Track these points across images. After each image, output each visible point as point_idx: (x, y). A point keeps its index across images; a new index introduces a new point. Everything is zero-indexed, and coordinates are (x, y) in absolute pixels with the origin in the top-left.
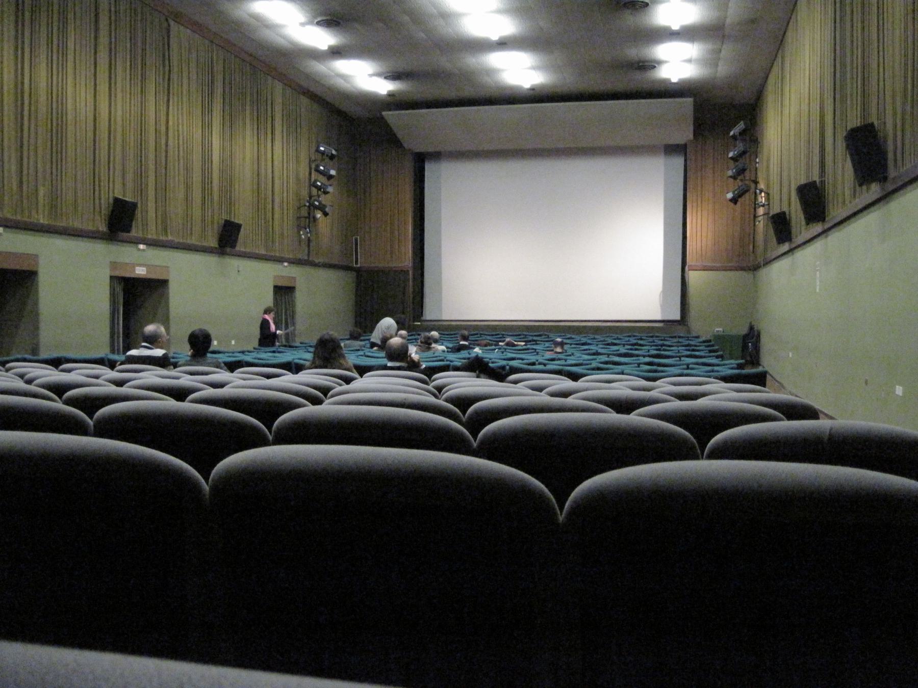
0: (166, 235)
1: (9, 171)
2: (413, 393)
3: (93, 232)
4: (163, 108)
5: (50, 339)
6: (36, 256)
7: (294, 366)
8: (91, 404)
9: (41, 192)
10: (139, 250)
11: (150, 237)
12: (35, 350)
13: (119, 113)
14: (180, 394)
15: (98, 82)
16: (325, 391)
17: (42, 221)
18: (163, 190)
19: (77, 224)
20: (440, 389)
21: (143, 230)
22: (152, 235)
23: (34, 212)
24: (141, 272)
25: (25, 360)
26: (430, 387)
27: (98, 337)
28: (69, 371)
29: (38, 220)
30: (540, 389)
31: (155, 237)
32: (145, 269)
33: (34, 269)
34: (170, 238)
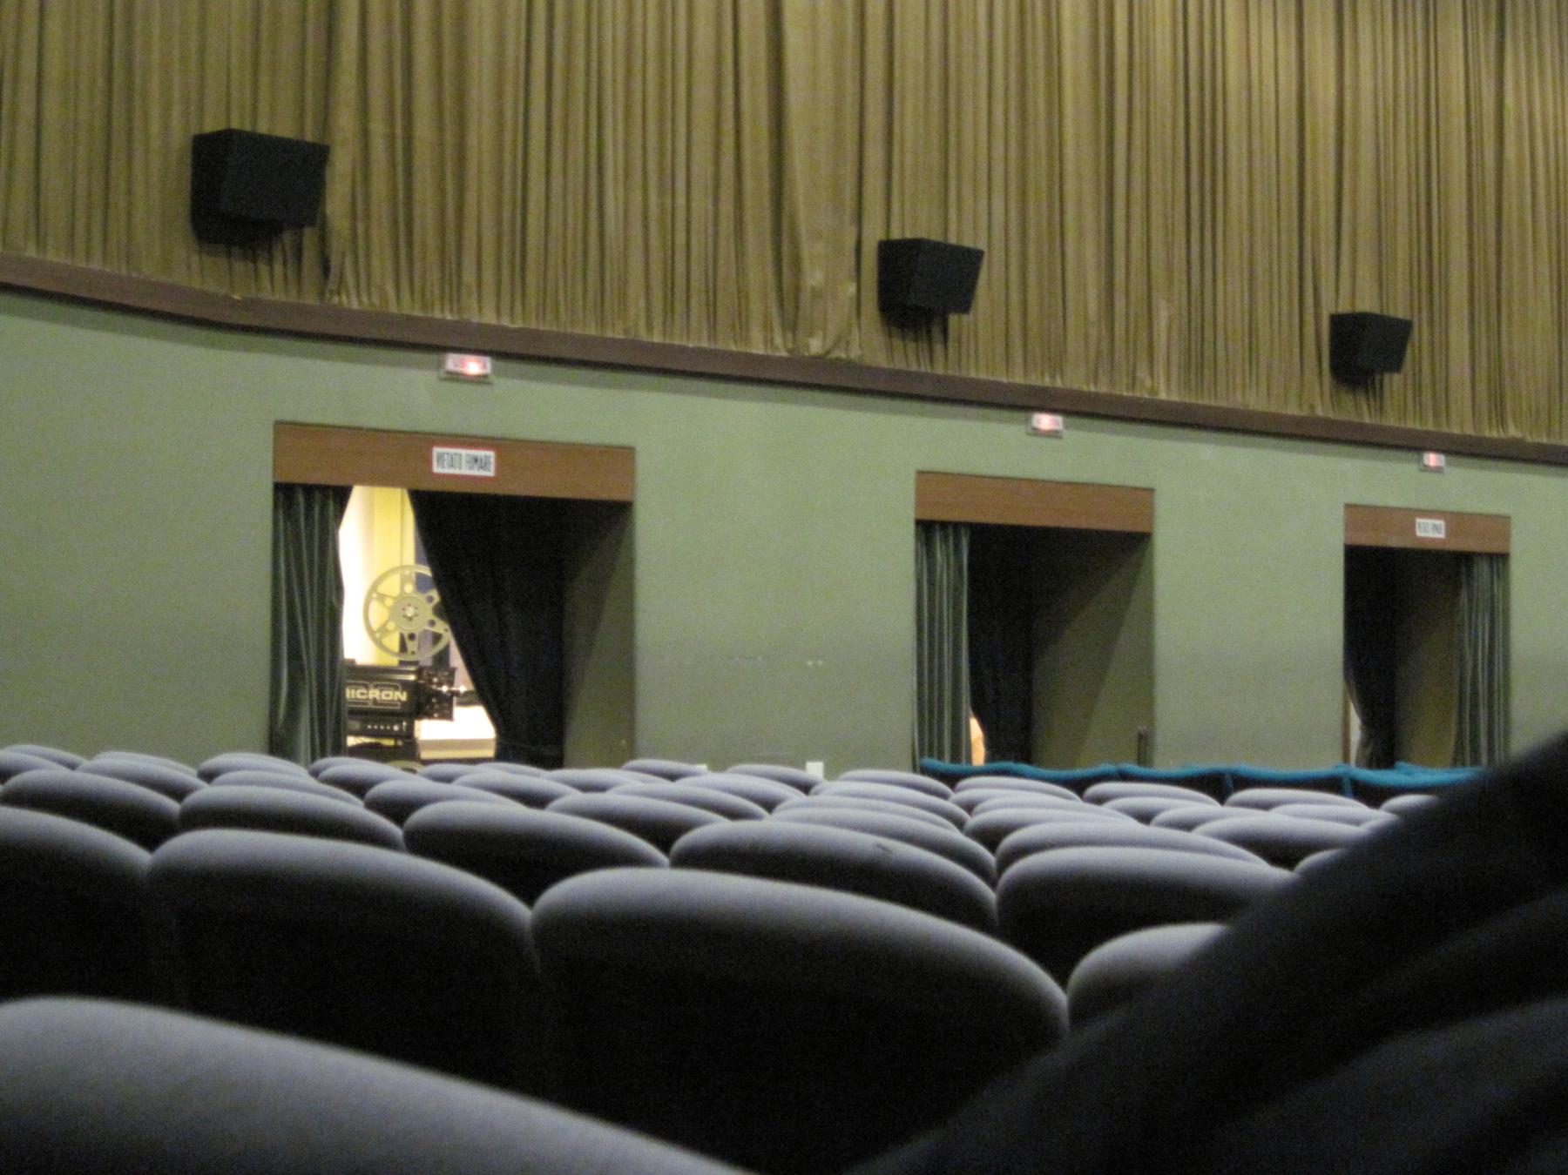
0: (1502, 422)
1: (1080, 257)
2: (893, 812)
3: (1299, 421)
4: (1487, 54)
5: (1184, 715)
6: (1150, 491)
7: (1346, 782)
8: (398, 809)
9: (1162, 315)
10: (1426, 469)
11: (1456, 430)
12: (1143, 747)
13: (1366, 83)
14: (537, 800)
15: (922, 25)
16: (770, 805)
17: (1163, 396)
18: (1490, 300)
19: (1254, 401)
20: (970, 807)
21: (1436, 415)
22: (1461, 425)
23: (1143, 372)
24: (1430, 531)
25: (1124, 777)
26: (948, 805)
27: (1329, 720)
28: (1266, 806)
29: (1153, 391)
30: (1145, 817)
31: (1469, 431)
32: (1441, 523)
33: (1147, 530)
34: (1513, 432)
